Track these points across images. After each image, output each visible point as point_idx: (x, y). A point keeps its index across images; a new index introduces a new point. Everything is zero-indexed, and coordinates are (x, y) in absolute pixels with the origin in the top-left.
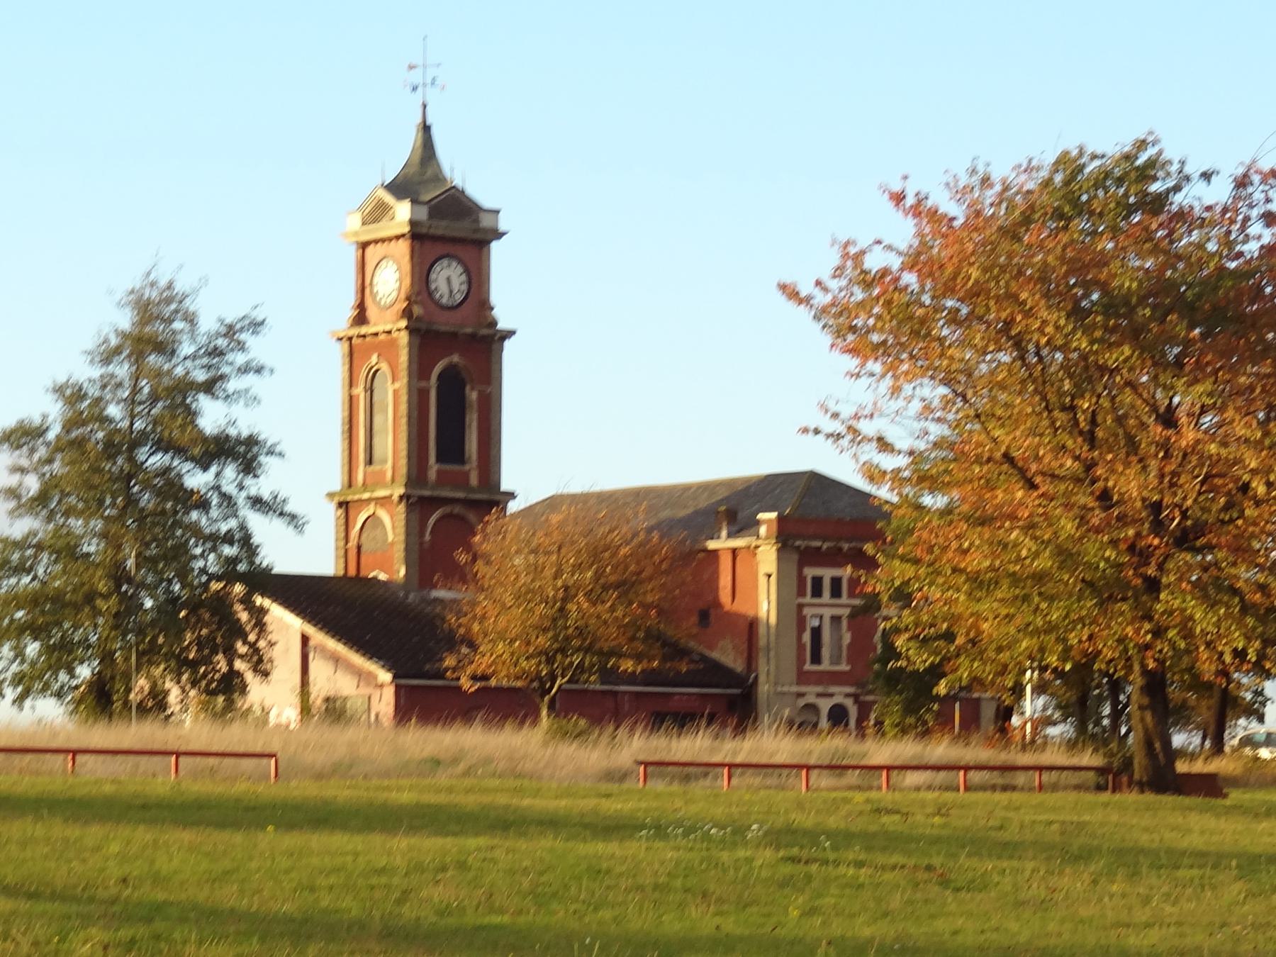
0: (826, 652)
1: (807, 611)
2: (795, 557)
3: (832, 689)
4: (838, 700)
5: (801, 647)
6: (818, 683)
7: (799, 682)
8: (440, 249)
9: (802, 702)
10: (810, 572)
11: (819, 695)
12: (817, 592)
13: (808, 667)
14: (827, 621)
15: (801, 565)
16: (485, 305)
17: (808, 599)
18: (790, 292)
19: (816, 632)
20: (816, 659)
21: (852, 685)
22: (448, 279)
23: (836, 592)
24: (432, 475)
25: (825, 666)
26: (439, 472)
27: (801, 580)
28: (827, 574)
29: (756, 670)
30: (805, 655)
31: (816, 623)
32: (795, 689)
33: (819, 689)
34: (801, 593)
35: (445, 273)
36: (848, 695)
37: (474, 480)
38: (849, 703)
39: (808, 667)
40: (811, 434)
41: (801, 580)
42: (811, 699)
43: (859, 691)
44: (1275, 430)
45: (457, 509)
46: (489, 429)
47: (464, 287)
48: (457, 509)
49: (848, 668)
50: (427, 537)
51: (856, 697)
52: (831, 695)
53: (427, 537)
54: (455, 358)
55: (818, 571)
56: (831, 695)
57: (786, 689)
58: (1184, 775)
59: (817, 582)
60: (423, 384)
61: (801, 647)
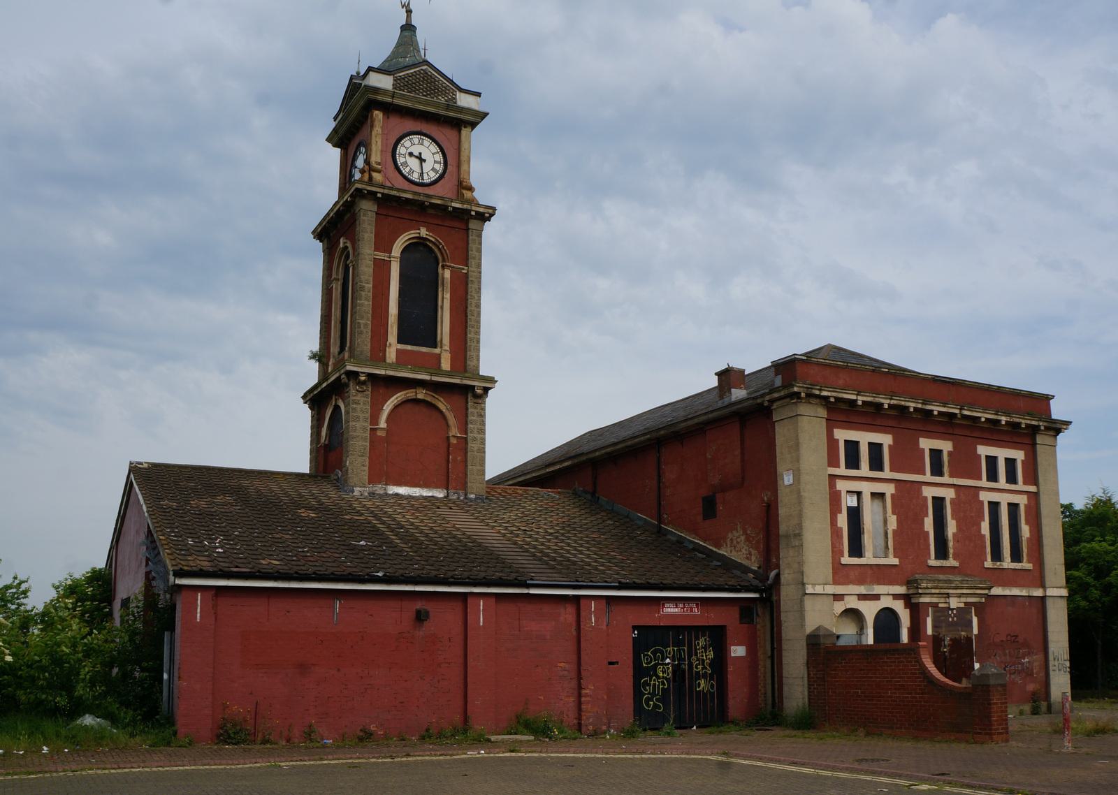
0: (868, 541)
1: (842, 486)
3: (878, 589)
4: (886, 602)
5: (836, 532)
6: (861, 582)
8: (410, 125)
9: (839, 607)
10: (842, 435)
11: (862, 597)
12: (853, 462)
13: (846, 559)
14: (866, 498)
15: (831, 424)
16: (463, 186)
17: (842, 470)
19: (855, 515)
20: (856, 550)
21: (901, 584)
23: (876, 464)
24: (391, 355)
25: (868, 558)
26: (398, 351)
27: (832, 443)
28: (864, 438)
29: (778, 566)
30: (125, 506)
31: (852, 501)
32: (831, 589)
33: (862, 590)
34: (833, 462)
36: (896, 597)
37: (446, 365)
38: (899, 606)
39: (846, 559)
41: (832, 443)
42: (852, 603)
43: (911, 591)
45: (421, 394)
46: (918, 624)
48: (421, 394)
49: (896, 561)
51: (907, 599)
52: (876, 597)
54: (424, 232)
55: (853, 435)
56: (876, 597)
57: (819, 589)
58: (380, 436)
59: (852, 447)
60: (382, 256)
61: (836, 532)
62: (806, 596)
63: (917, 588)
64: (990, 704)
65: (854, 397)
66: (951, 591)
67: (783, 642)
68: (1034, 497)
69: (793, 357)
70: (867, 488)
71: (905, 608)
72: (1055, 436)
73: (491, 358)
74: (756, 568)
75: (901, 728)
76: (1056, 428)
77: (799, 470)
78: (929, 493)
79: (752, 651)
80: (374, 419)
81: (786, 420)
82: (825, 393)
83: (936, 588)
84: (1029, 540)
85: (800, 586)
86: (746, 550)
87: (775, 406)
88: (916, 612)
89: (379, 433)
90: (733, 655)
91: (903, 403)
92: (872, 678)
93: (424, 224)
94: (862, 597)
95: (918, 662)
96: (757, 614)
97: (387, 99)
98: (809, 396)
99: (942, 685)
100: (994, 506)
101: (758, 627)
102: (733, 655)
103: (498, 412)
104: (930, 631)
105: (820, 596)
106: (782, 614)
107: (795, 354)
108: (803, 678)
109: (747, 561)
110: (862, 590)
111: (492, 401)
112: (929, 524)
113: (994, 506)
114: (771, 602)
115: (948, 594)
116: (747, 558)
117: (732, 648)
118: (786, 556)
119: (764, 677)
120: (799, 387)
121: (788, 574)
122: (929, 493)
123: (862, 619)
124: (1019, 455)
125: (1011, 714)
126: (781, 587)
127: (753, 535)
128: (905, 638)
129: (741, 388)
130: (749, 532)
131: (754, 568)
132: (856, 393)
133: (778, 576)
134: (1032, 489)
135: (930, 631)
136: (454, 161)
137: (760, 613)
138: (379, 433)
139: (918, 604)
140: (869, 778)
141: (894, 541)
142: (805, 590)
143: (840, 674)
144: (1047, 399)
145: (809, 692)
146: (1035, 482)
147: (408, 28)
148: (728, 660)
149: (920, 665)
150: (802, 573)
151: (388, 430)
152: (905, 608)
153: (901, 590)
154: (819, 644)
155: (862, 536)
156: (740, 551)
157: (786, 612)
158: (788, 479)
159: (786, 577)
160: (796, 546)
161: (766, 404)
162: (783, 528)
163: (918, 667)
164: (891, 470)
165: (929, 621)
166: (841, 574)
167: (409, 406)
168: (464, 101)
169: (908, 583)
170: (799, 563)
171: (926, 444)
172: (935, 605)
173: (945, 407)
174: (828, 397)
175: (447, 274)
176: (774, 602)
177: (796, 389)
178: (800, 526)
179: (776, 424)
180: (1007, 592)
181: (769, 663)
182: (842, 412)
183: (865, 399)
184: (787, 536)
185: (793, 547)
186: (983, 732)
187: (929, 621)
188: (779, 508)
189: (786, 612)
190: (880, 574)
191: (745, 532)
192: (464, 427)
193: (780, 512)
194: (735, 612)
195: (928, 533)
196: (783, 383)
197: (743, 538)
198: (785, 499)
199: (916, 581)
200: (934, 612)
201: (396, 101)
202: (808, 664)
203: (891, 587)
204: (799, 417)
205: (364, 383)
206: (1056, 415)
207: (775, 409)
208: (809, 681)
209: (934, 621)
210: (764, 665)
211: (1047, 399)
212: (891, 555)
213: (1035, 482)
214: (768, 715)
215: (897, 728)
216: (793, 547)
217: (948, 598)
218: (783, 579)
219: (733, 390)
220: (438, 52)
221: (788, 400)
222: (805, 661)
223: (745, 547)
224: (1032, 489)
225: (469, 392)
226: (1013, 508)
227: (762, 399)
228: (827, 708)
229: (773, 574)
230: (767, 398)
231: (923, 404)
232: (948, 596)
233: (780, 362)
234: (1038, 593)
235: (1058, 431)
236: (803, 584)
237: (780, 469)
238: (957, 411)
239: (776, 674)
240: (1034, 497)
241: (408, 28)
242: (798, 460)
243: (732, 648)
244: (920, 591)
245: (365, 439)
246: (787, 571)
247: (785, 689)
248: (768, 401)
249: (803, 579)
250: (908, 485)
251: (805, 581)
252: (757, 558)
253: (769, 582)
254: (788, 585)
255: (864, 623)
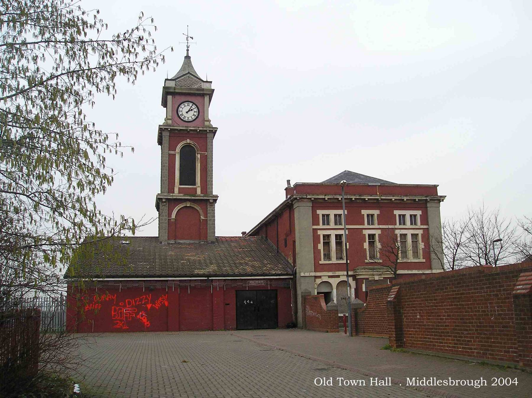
1: (321, 233)
2: (310, 204)
3: (337, 273)
8: (183, 99)
9: (319, 281)
11: (330, 277)
18: (288, 182)
20: (328, 256)
22: (188, 112)
32: (313, 274)
33: (330, 274)
35: (187, 115)
40: (155, 23)
44: (1, 54)
47: (186, 104)
49: (424, 261)
50: (173, 216)
52: (338, 276)
53: (173, 216)
54: (188, 141)
56: (338, 276)
57: (307, 274)
68: (426, 231)
73: (218, 188)
76: (441, 199)
78: (366, 233)
80: (170, 215)
82: (308, 197)
87: (294, 202)
89: (172, 220)
93: (188, 138)
94: (330, 277)
97: (172, 91)
100: (404, 236)
103: (220, 210)
104: (364, 290)
110: (330, 274)
111: (218, 206)
112: (366, 245)
113: (404, 236)
122: (366, 233)
124: (419, 213)
125: (341, 313)
134: (425, 227)
135: (364, 290)
136: (202, 113)
138: (172, 220)
144: (435, 187)
146: (427, 224)
147: (188, 57)
151: (176, 219)
165: (364, 286)
166: (318, 267)
167: (184, 209)
168: (205, 86)
171: (365, 212)
172: (367, 279)
174: (311, 198)
175: (199, 156)
180: (410, 272)
182: (317, 204)
183: (329, 197)
187: (364, 286)
192: (206, 215)
201: (176, 91)
205: (165, 202)
206: (439, 194)
211: (435, 187)
213: (427, 224)
220: (202, 71)
224: (425, 227)
225: (209, 202)
235: (439, 201)
240: (426, 231)
241: (188, 57)
245: (166, 223)
250: (355, 230)
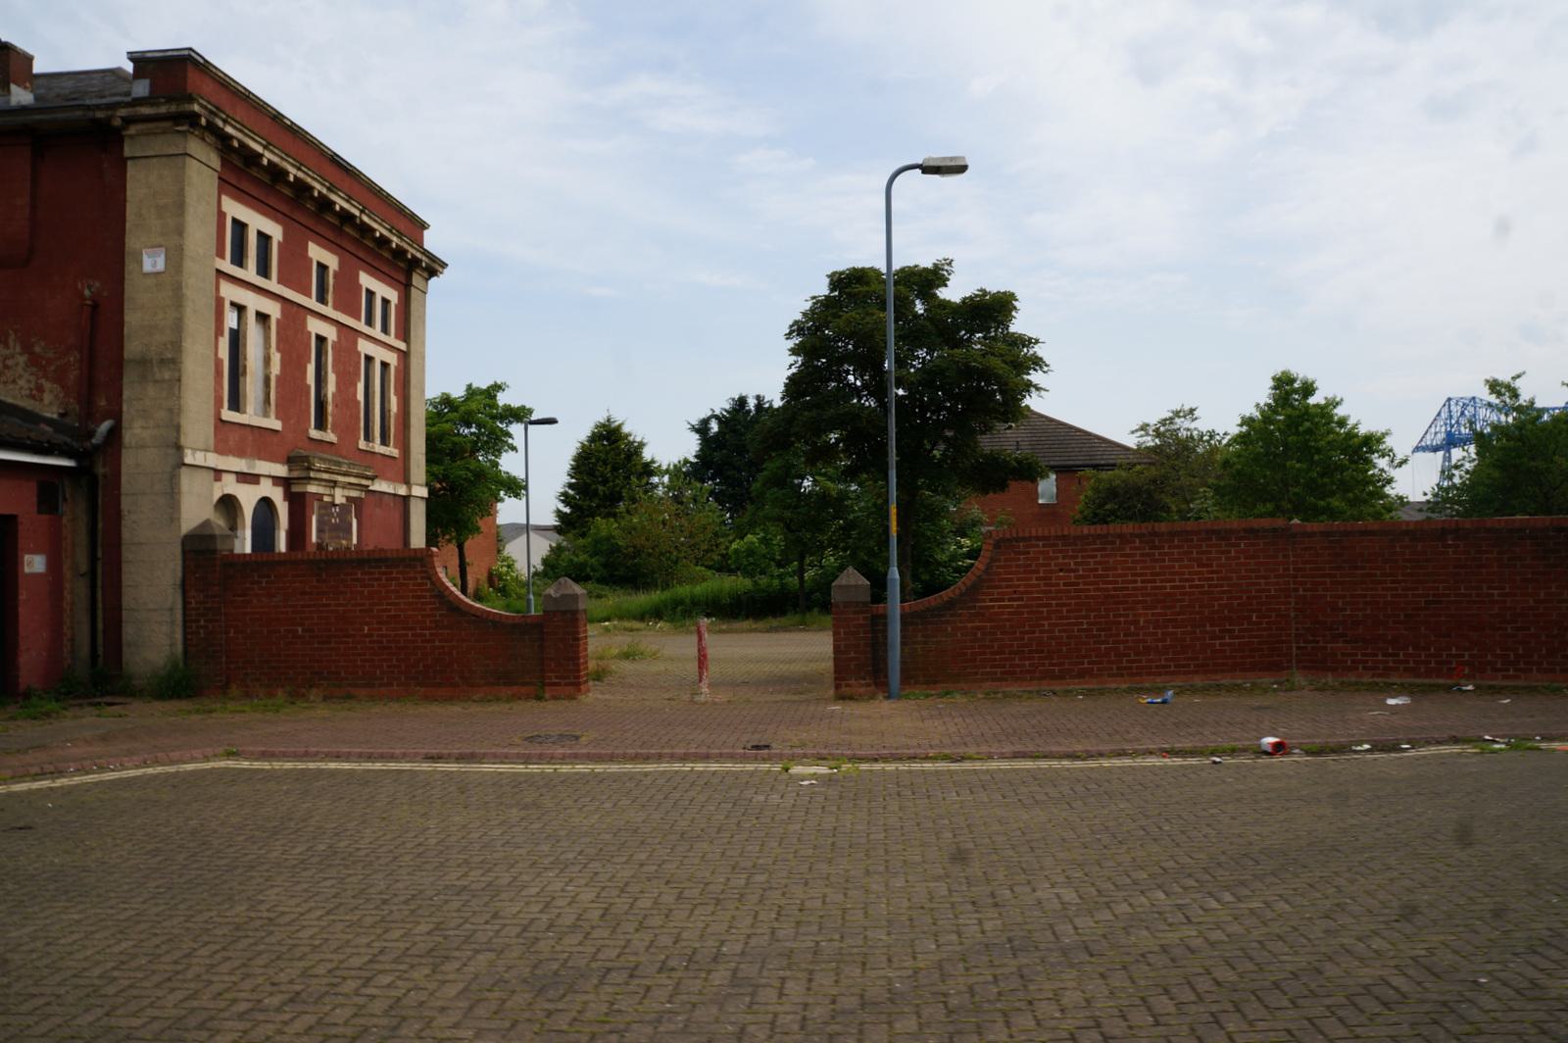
0: (252, 388)
4: (267, 489)
5: (218, 363)
7: (221, 449)
19: (237, 339)
20: (236, 404)
33: (240, 465)
36: (277, 480)
38: (277, 495)
42: (230, 486)
43: (295, 474)
49: (277, 425)
62: (184, 469)
63: (309, 469)
64: (578, 639)
65: (260, 149)
66: (340, 478)
67: (124, 548)
69: (186, 53)
70: (254, 302)
71: (40, 512)
72: (427, 280)
74: (55, 416)
75: (390, 684)
77: (180, 249)
79: (54, 564)
81: (154, 160)
82: (229, 130)
83: (326, 471)
84: (397, 415)
85: (172, 451)
86: (29, 381)
87: (133, 130)
88: (298, 503)
90: (27, 570)
91: (309, 180)
92: (329, 605)
95: (429, 578)
96: (65, 499)
98: (211, 128)
99: (479, 614)
101: (65, 520)
102: (27, 570)
104: (314, 539)
105: (200, 470)
106: (123, 498)
107: (191, 49)
108: (171, 609)
109: (32, 402)
110: (240, 465)
114: (94, 478)
115: (335, 482)
116: (33, 397)
117: (27, 557)
118: (138, 399)
119: (71, 610)
120: (201, 105)
121: (143, 427)
123: (235, 507)
126: (123, 451)
127: (51, 355)
128: (282, 545)
129: (25, 88)
130: (37, 349)
131: (48, 415)
132: (264, 143)
133: (115, 433)
135: (314, 539)
137: (68, 496)
139: (303, 495)
140: (301, 766)
141: (277, 393)
142: (182, 457)
143: (255, 601)
144: (423, 226)
145: (185, 634)
148: (20, 581)
149: (433, 583)
150: (178, 428)
152: (40, 512)
153: (281, 470)
154: (214, 551)
155: (241, 379)
156: (14, 381)
157: (133, 494)
158: (153, 262)
159: (135, 431)
160: (163, 381)
161: (117, 122)
162: (132, 348)
163: (429, 586)
164: (280, 281)
169: (290, 461)
170: (171, 411)
172: (319, 497)
173: (347, 201)
174: (231, 137)
176: (100, 478)
177: (196, 108)
178: (177, 345)
179: (129, 163)
181: (82, 588)
184: (144, 362)
185: (156, 381)
186: (562, 682)
188: (126, 311)
189: (133, 494)
190: (256, 442)
191: (27, 348)
193: (127, 318)
194: (29, 491)
195: (309, 387)
196: (151, 92)
197: (22, 359)
198: (135, 292)
199: (306, 458)
200: (320, 508)
202: (185, 586)
203: (272, 465)
204: (188, 159)
207: (131, 137)
208: (185, 615)
209: (318, 521)
210: (76, 591)
211: (423, 226)
212: (273, 416)
214: (99, 677)
215: (381, 685)
216: (156, 381)
217: (333, 487)
218: (128, 437)
219: (13, 88)
221: (167, 124)
222: (178, 581)
223: (26, 375)
224: (402, 346)
226: (385, 365)
227: (110, 113)
228: (224, 659)
229: (105, 426)
230: (123, 112)
231: (329, 189)
232: (334, 484)
233: (149, 55)
234: (402, 491)
236: (179, 448)
237: (132, 242)
238: (357, 213)
239: (100, 605)
242: (180, 231)
243: (27, 557)
244: (312, 474)
246: (138, 424)
247: (128, 631)
248: (122, 118)
249: (178, 438)
251: (183, 441)
252: (56, 396)
253: (94, 441)
254: (143, 447)
255: (239, 521)
